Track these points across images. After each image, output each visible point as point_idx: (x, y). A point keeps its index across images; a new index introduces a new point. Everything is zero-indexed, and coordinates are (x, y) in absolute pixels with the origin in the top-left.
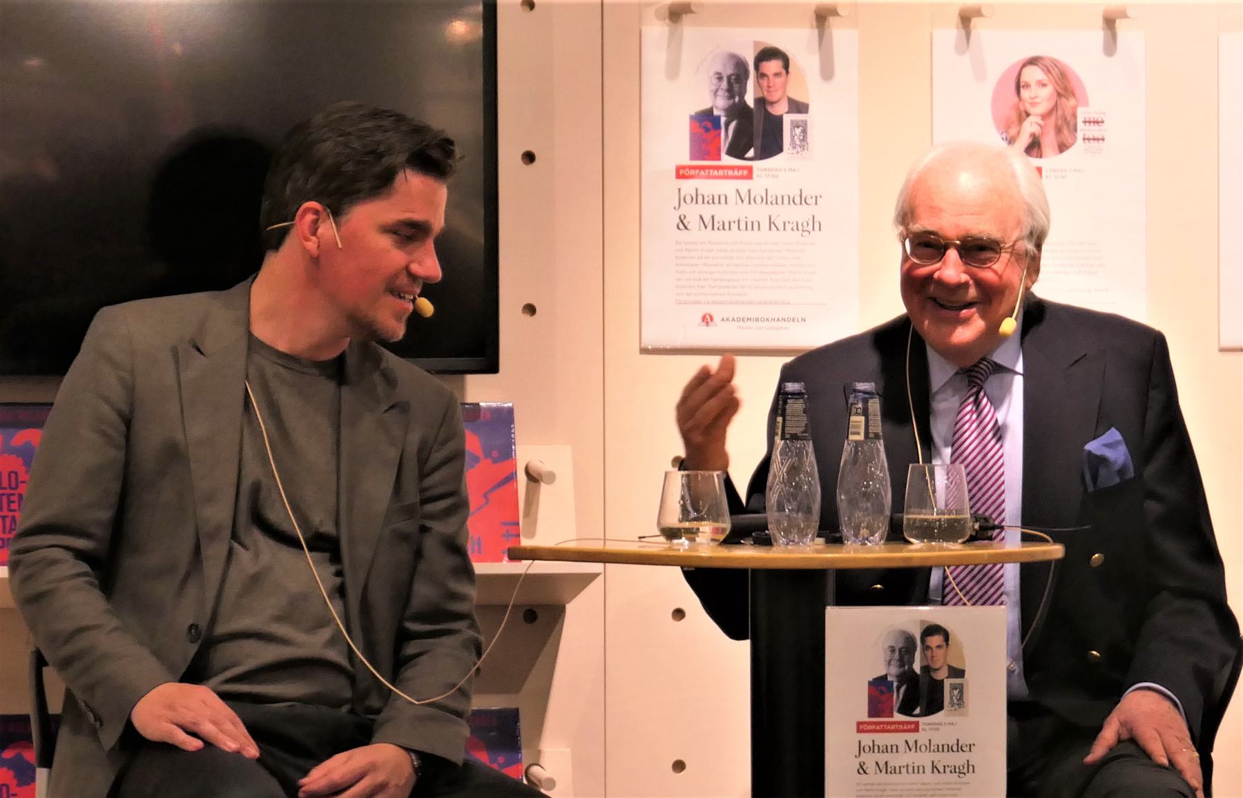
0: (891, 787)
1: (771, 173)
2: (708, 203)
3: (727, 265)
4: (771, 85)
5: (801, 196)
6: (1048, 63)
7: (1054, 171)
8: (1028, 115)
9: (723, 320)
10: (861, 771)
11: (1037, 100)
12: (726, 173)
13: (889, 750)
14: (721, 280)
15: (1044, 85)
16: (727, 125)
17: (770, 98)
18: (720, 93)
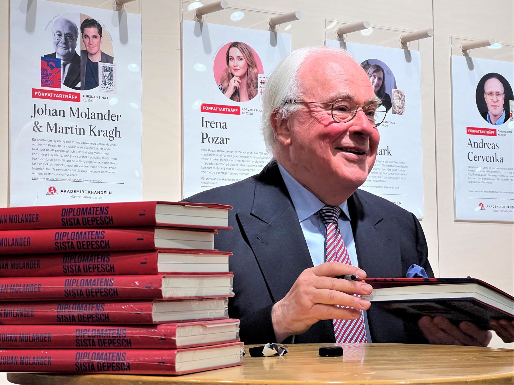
0: (60, 144)
1: (91, 99)
2: (53, 115)
3: (65, 156)
4: (91, 43)
5: (109, 115)
6: (243, 47)
7: (246, 110)
8: (233, 76)
9: (62, 191)
10: (36, 129)
11: (237, 68)
12: (64, 97)
13: (58, 114)
14: (61, 165)
15: (241, 59)
16: (64, 66)
17: (90, 51)
18: (60, 44)
